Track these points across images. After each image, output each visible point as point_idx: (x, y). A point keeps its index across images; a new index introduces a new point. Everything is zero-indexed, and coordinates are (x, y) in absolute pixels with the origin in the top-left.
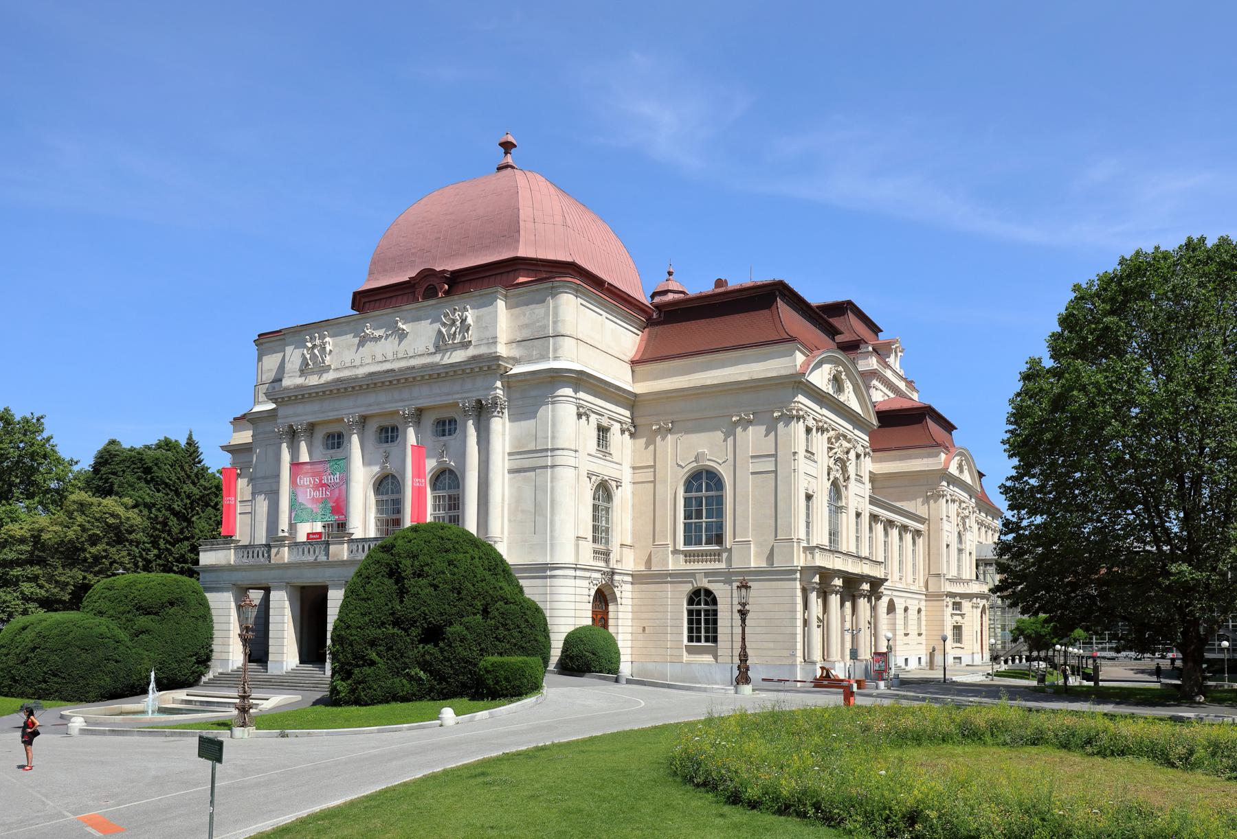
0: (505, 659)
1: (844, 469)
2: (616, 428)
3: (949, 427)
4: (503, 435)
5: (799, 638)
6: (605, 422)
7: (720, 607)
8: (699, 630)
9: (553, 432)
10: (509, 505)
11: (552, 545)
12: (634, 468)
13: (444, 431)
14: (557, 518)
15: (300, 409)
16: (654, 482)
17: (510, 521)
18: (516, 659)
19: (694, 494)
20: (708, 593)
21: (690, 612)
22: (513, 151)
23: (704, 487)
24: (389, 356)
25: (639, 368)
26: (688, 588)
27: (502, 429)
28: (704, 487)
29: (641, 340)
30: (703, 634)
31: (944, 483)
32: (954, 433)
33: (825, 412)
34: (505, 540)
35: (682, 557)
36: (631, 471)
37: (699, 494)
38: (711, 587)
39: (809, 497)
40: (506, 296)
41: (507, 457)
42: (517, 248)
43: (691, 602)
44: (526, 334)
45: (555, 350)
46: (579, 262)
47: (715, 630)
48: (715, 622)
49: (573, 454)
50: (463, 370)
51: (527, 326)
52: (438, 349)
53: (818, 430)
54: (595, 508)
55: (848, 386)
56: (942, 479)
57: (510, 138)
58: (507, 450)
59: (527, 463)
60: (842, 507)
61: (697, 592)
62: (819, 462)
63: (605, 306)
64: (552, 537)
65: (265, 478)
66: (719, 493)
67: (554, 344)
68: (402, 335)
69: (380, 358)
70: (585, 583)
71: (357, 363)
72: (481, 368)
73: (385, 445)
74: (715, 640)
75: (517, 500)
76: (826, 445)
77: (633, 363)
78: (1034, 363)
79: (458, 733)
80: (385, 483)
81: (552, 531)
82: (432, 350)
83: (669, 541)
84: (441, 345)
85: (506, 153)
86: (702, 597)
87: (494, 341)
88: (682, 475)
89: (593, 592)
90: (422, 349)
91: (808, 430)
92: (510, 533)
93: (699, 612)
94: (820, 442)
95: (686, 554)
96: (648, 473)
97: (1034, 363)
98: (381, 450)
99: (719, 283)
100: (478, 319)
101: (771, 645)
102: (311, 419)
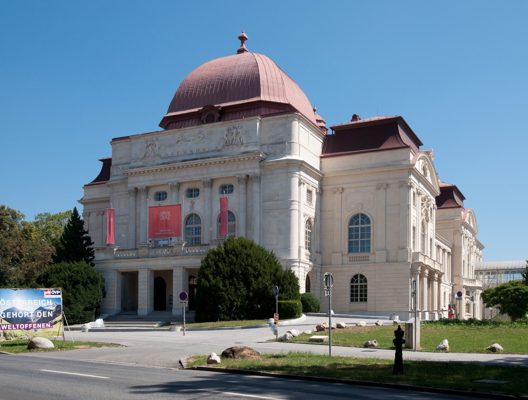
0: (288, 301)
3: (462, 198)
6: (310, 188)
7: (368, 284)
8: (357, 296)
13: (160, 198)
15: (141, 178)
18: (291, 301)
19: (354, 226)
20: (362, 276)
21: (352, 287)
22: (246, 42)
24: (194, 151)
30: (359, 298)
31: (463, 227)
32: (464, 201)
33: (421, 185)
38: (364, 274)
42: (259, 95)
43: (352, 281)
46: (291, 103)
47: (366, 295)
48: (366, 291)
56: (462, 225)
57: (245, 35)
61: (356, 276)
63: (310, 128)
65: (119, 216)
71: (175, 154)
72: (249, 158)
73: (192, 198)
74: (366, 300)
78: (71, 211)
79: (258, 340)
80: (191, 218)
85: (242, 43)
86: (359, 279)
88: (348, 215)
90: (213, 148)
93: (357, 286)
97: (71, 211)
98: (190, 201)
99: (355, 117)
102: (148, 184)
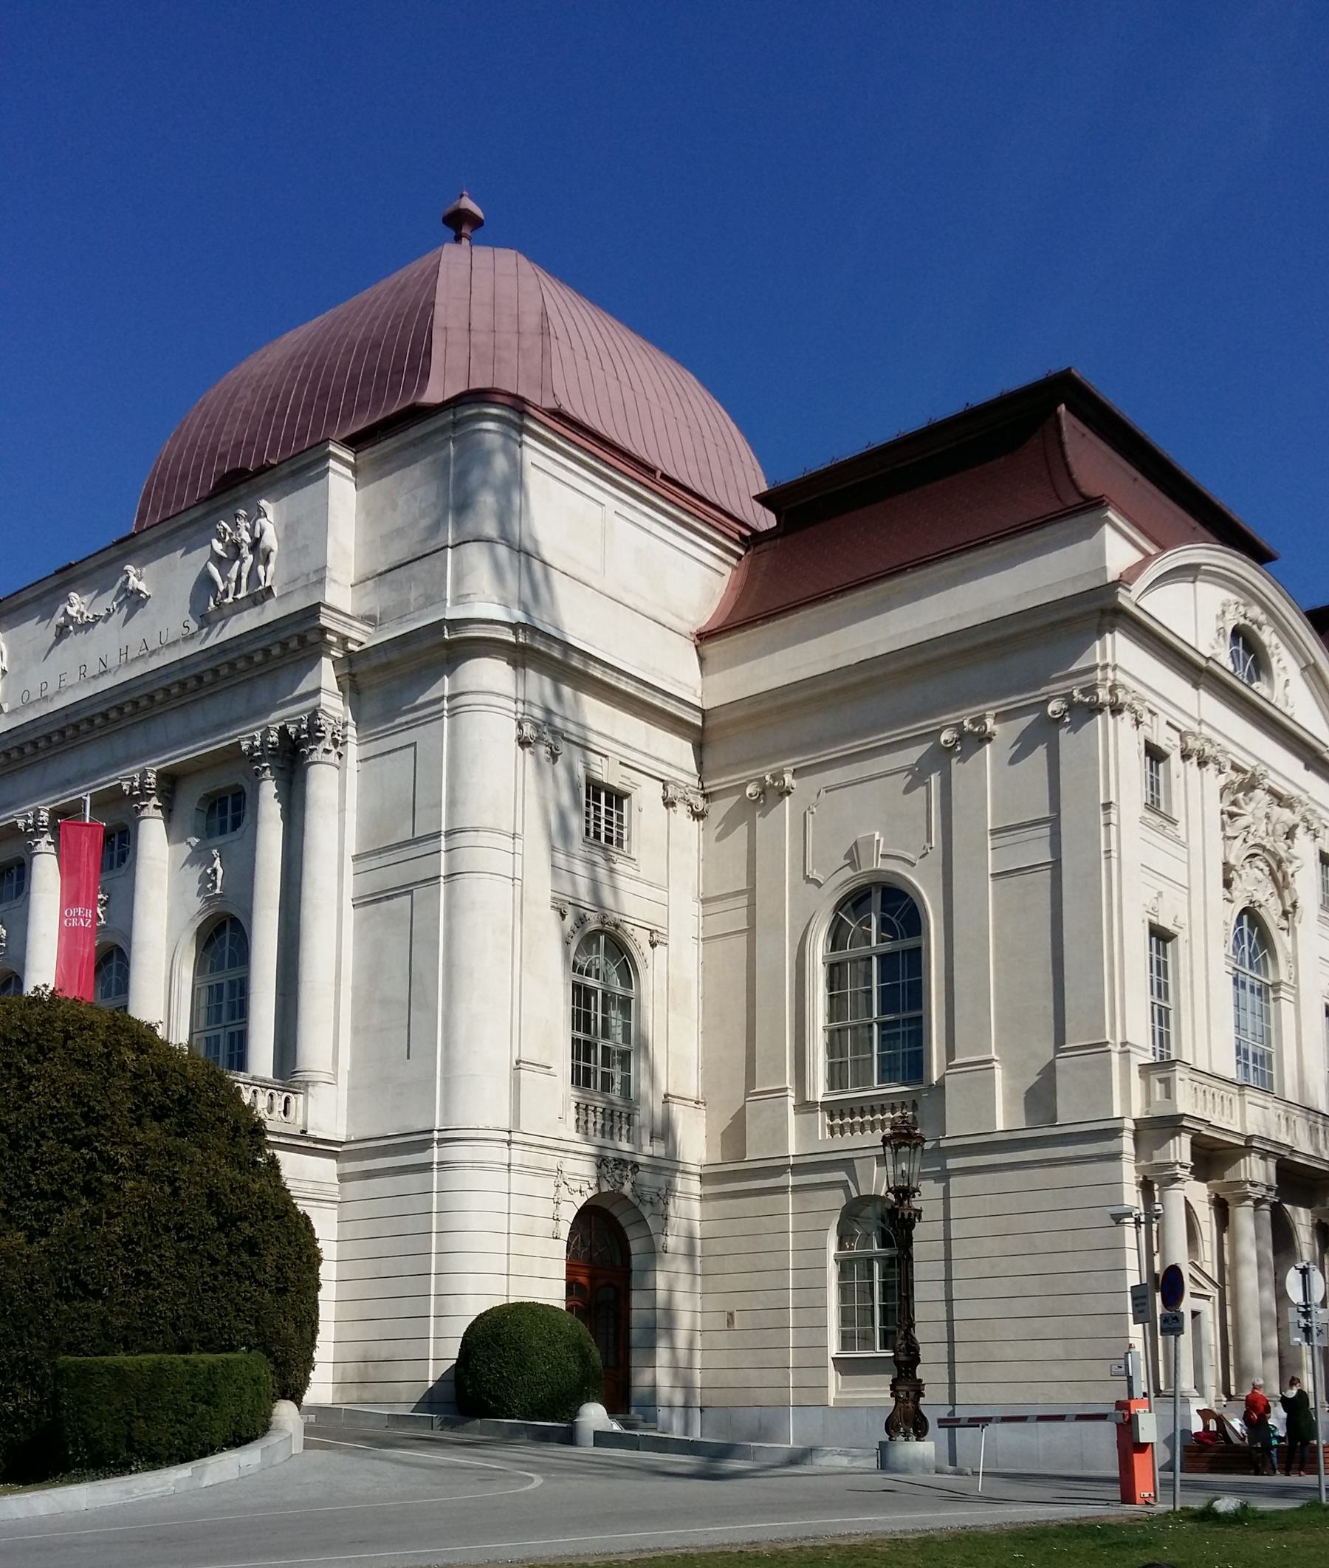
1: (1281, 883)
2: (646, 796)
4: (342, 810)
5: (1232, 1382)
9: (452, 789)
10: (355, 989)
11: (447, 1081)
12: (704, 901)
14: (461, 1012)
16: (751, 931)
17: (355, 1031)
23: (884, 932)
24: (113, 661)
25: (712, 648)
26: (836, 1200)
27: (340, 793)
28: (884, 932)
29: (730, 588)
34: (343, 1080)
35: (821, 1118)
36: (696, 908)
37: (862, 950)
39: (1160, 936)
40: (355, 469)
41: (349, 866)
44: (399, 552)
45: (458, 580)
49: (507, 843)
50: (249, 658)
51: (399, 532)
52: (205, 620)
53: (1185, 756)
54: (581, 995)
55: (1284, 663)
58: (352, 848)
59: (394, 877)
60: (1276, 986)
62: (1196, 842)
64: (447, 1062)
66: (908, 943)
67: (457, 564)
68: (134, 601)
69: (94, 668)
70: (545, 1186)
72: (284, 645)
75: (371, 972)
76: (1215, 806)
77: (703, 637)
81: (446, 1046)
82: (194, 626)
83: (789, 1082)
84: (206, 602)
87: (319, 578)
89: (569, 1213)
90: (176, 631)
91: (1155, 754)
92: (354, 1062)
94: (1197, 792)
95: (832, 1109)
96: (740, 910)
100: (288, 531)
101: (1057, 1349)
